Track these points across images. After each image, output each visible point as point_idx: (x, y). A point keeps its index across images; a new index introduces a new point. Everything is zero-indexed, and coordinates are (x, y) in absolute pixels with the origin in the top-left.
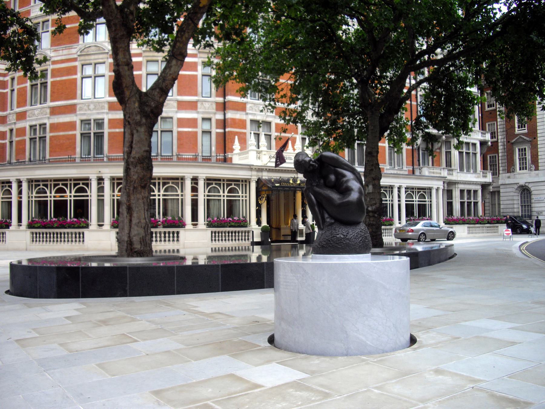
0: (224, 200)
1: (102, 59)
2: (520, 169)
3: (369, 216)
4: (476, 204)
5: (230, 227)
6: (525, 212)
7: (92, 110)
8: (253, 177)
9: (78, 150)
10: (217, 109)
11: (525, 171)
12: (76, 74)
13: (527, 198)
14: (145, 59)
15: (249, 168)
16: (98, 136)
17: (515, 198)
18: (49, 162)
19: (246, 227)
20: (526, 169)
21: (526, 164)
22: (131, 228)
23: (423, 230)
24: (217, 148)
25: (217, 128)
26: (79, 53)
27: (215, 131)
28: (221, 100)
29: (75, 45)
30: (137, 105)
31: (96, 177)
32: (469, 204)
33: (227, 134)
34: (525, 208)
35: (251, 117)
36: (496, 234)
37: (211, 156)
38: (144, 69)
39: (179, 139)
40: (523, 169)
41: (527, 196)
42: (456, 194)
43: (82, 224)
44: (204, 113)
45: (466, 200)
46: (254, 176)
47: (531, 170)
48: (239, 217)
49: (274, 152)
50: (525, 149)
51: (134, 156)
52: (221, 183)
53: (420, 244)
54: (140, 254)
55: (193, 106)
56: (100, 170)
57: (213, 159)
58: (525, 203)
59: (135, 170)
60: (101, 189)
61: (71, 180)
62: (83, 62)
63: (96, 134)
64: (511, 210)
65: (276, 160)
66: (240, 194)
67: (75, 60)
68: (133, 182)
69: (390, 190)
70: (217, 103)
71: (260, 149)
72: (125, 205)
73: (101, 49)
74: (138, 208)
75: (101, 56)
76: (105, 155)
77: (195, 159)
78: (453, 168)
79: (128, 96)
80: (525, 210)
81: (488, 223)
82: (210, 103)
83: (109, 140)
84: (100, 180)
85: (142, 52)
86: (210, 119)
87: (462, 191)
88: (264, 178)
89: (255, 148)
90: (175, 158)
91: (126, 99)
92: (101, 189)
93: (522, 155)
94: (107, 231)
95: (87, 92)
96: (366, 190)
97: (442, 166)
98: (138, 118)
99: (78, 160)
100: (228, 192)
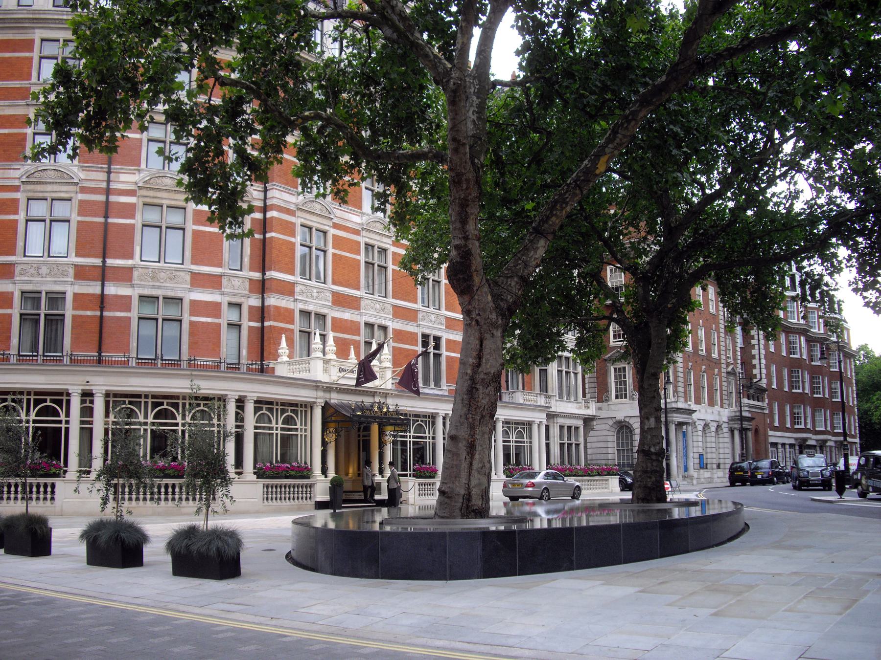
0: (277, 434)
1: (66, 192)
2: (617, 397)
3: (652, 459)
4: (577, 445)
5: (287, 477)
6: (624, 459)
7: (44, 275)
8: (319, 400)
9: (15, 341)
10: (251, 291)
11: (624, 400)
12: (16, 212)
13: (627, 439)
14: (142, 200)
15: (313, 386)
16: (52, 320)
17: (610, 439)
18: (190, 365)
19: (308, 477)
20: (626, 397)
21: (625, 390)
22: (470, 475)
23: (545, 483)
24: (249, 352)
25: (250, 320)
26: (24, 179)
27: (247, 324)
28: (257, 275)
29: (16, 165)
30: (490, 297)
31: (80, 391)
32: (570, 445)
33: (266, 331)
34: (623, 453)
35: (301, 306)
36: (606, 490)
37: (180, 360)
38: (138, 216)
39: (191, 334)
40: (621, 398)
41: (627, 437)
42: (555, 431)
43: (53, 470)
44: (231, 294)
45: (566, 441)
46: (319, 398)
47: (633, 399)
48: (271, 463)
49: (353, 361)
50: (624, 368)
51: (488, 371)
52: (273, 408)
53: (542, 504)
54: (480, 513)
55: (214, 282)
56: (88, 378)
57: (244, 369)
58: (623, 446)
59: (487, 391)
60: (87, 412)
61: (29, 394)
62: (30, 194)
63: (48, 317)
64: (602, 457)
65: (359, 375)
66: (298, 426)
67: (16, 189)
68: (482, 409)
69: (431, 420)
70: (251, 281)
71: (328, 357)
72: (464, 442)
73: (66, 176)
74: (481, 446)
75: (65, 188)
76: (65, 354)
77: (217, 367)
78: (550, 393)
79: (478, 284)
80: (623, 457)
81: (599, 475)
82: (241, 280)
83: (73, 328)
84: (87, 395)
85: (136, 188)
86: (239, 306)
87: (561, 427)
88: (333, 401)
89: (321, 355)
90: (184, 365)
91: (475, 288)
92: (87, 412)
93: (620, 378)
94: (250, 482)
95: (35, 246)
96: (645, 424)
97: (534, 390)
98: (493, 316)
99: (13, 359)
100: (283, 423)
